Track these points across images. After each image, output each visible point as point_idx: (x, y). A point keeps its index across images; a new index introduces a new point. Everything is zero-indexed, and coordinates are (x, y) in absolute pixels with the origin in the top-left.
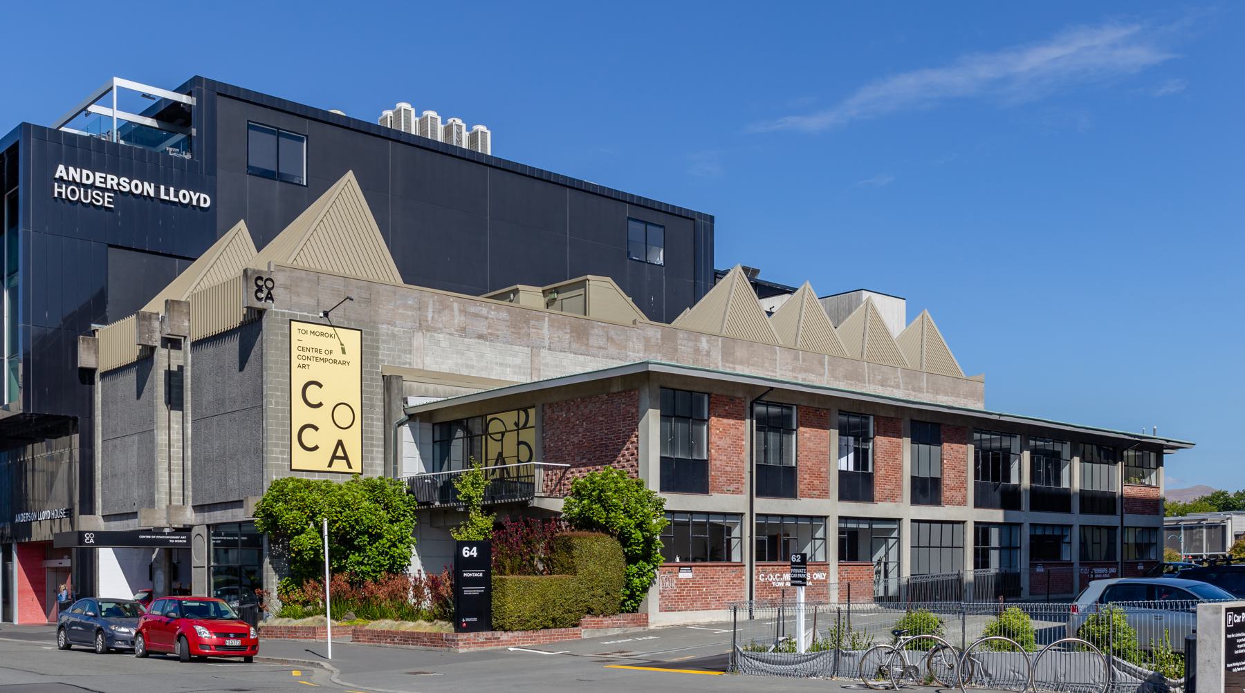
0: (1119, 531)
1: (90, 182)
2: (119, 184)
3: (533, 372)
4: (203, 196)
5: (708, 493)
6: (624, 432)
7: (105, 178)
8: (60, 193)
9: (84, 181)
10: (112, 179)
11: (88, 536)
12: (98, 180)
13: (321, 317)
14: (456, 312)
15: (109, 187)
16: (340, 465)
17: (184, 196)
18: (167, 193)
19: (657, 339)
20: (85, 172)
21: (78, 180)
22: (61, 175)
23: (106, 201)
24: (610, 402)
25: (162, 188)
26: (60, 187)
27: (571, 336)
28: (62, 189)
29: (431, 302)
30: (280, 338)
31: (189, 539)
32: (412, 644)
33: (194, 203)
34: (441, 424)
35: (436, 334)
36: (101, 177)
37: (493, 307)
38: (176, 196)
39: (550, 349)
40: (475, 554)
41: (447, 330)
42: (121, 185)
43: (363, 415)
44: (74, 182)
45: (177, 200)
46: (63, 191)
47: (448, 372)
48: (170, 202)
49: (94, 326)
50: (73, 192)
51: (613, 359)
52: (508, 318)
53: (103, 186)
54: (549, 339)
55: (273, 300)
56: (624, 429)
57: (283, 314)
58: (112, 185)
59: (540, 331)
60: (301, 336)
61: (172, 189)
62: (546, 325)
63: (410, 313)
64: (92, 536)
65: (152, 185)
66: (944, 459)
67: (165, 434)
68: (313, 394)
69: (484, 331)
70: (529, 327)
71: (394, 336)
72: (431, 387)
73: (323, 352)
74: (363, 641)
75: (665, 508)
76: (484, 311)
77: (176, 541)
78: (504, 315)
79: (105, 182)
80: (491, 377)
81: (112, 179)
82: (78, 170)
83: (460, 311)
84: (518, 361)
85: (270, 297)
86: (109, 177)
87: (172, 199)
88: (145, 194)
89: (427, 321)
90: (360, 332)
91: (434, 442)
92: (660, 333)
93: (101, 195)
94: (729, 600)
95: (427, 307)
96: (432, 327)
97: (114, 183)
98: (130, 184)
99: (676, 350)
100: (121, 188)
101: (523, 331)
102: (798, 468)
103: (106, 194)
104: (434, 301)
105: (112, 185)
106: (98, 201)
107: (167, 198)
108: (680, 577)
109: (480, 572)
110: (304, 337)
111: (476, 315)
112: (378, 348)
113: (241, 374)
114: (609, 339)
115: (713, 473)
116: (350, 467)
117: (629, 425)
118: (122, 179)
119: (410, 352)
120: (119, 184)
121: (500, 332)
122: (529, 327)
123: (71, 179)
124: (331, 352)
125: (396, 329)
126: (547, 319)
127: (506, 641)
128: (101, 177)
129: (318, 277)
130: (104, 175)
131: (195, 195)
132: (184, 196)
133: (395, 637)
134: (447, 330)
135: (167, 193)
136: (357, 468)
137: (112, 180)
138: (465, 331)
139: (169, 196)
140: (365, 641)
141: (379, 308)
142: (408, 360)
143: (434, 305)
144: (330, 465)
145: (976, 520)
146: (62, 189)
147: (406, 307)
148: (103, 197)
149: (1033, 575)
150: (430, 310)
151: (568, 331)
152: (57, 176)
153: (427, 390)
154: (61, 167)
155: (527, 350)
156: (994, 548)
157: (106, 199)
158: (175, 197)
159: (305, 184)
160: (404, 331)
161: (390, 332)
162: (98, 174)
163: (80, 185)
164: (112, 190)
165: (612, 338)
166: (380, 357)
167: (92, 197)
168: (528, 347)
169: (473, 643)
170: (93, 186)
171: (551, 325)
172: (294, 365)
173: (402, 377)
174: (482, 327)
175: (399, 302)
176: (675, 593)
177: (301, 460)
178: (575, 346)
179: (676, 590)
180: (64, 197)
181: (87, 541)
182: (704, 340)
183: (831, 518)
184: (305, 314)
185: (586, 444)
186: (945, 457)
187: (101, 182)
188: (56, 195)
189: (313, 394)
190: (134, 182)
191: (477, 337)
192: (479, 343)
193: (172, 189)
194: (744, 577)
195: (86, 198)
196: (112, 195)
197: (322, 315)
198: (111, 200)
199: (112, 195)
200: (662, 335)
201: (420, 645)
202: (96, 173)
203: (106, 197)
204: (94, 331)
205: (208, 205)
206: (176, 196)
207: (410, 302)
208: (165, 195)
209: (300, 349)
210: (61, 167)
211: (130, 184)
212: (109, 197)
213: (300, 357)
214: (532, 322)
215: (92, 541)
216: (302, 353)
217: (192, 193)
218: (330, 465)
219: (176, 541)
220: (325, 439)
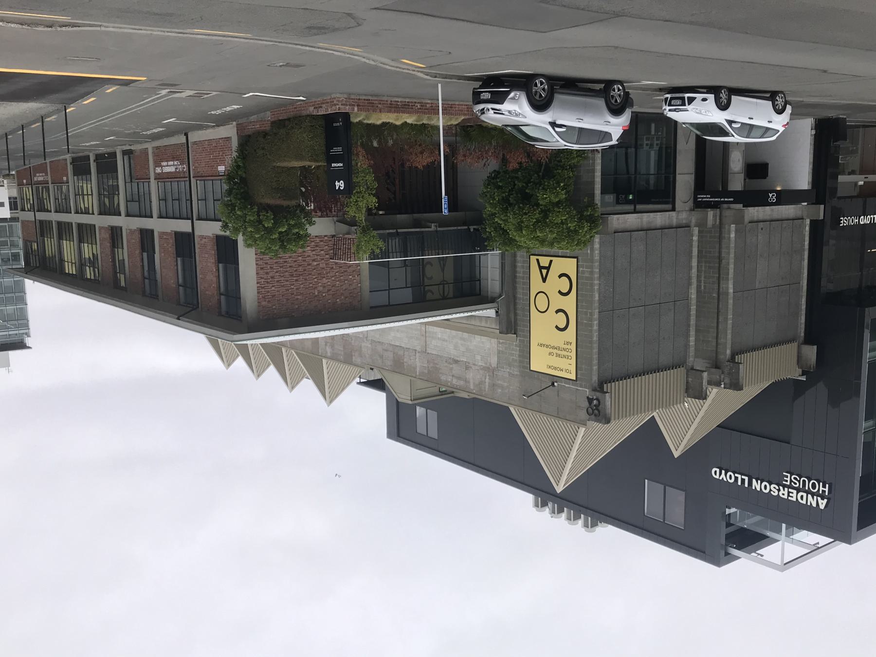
0: (36, 208)
1: (800, 494)
2: (779, 490)
3: (425, 334)
4: (717, 477)
5: (216, 236)
6: (273, 286)
7: (789, 496)
8: (824, 486)
9: (805, 495)
10: (783, 494)
11: (774, 200)
12: (794, 495)
13: (556, 382)
14: (471, 381)
15: (786, 489)
16: (545, 261)
17: (731, 478)
18: (743, 481)
19: (354, 356)
20: (804, 502)
21: (810, 496)
22: (822, 501)
23: (788, 479)
24: (289, 310)
25: (746, 485)
26: (824, 491)
27: (403, 360)
28: (822, 490)
29: (487, 390)
30: (583, 366)
31: (695, 198)
32: (398, 102)
33: (723, 472)
34: (476, 295)
35: (484, 365)
36: (792, 497)
37: (449, 384)
38: (736, 478)
39: (416, 350)
40: (337, 183)
41: (477, 367)
42: (777, 490)
43: (528, 303)
44: (813, 495)
45: (736, 475)
46: (821, 488)
47: (476, 336)
48: (742, 474)
49: (804, 378)
50: (814, 486)
51: (379, 342)
52: (440, 375)
53: (790, 490)
54: (416, 359)
55: (588, 397)
56: (273, 288)
57: (581, 387)
58: (784, 490)
59: (422, 365)
60: (569, 367)
61: (739, 483)
62: (418, 370)
63: (499, 382)
64: (770, 200)
65: (754, 488)
66: (112, 262)
67: (723, 288)
68: (561, 321)
69: (454, 366)
70: (428, 367)
71: (510, 365)
72: (483, 324)
73: (555, 354)
74: (462, 105)
75: (220, 223)
76: (455, 381)
77: (705, 196)
78: (443, 378)
79: (789, 492)
80: (450, 330)
81: (783, 494)
82: (809, 504)
83: (469, 382)
84: (434, 342)
85: (590, 400)
86: (785, 497)
87: (739, 476)
88: (759, 481)
89: (489, 375)
90: (531, 369)
91: (480, 280)
92: (353, 360)
93: (792, 483)
94: (199, 148)
95: (489, 386)
96: (485, 370)
97: (782, 492)
98: (771, 490)
99: (344, 347)
100: (777, 488)
101: (432, 365)
102: (175, 256)
103: (788, 483)
104: (485, 391)
105: (784, 490)
106: (795, 478)
107: (743, 477)
108: (224, 167)
109: (333, 167)
110: (567, 368)
111: (459, 378)
112: (520, 356)
113: (33, 348)
114: (381, 357)
115: (213, 252)
116: (538, 260)
117: (268, 292)
118: (776, 494)
119: (499, 352)
120: (779, 490)
121: (445, 365)
122: (428, 367)
123: (815, 497)
124: (550, 354)
125: (508, 370)
126: (418, 374)
127: (310, 106)
128: (792, 497)
129: (558, 414)
130: (790, 498)
131: (723, 478)
132: (731, 478)
133: (420, 109)
134: (477, 367)
135: (743, 481)
136: (533, 259)
137: (784, 493)
138: (466, 367)
139: (742, 479)
140: (458, 105)
141: (519, 387)
142: (500, 345)
143: (485, 388)
144: (551, 261)
145: (70, 214)
146: (822, 490)
147: (502, 387)
148: (791, 481)
149: (67, 176)
150: (487, 384)
151: (405, 364)
152: (826, 500)
153: (486, 322)
154: (822, 507)
155: (429, 351)
156: (635, 207)
157: (789, 479)
158: (738, 477)
159: (646, 481)
160: (503, 368)
161: (512, 368)
162: (794, 499)
163: (808, 492)
164: (784, 486)
165: (380, 357)
166: (518, 349)
167: (799, 481)
168: (428, 353)
169: (328, 103)
170: (798, 490)
171: (415, 368)
172: (574, 346)
173: (500, 333)
174: (457, 370)
175: (506, 391)
176: (226, 153)
177: (569, 266)
178: (401, 353)
179: (226, 155)
180: (821, 484)
181: (774, 195)
182: (329, 354)
183: (156, 217)
184: (567, 385)
185: (314, 277)
186: (111, 264)
187: (792, 493)
188: (827, 485)
189: (561, 321)
190: (767, 491)
191: (459, 361)
192: (457, 357)
193: (739, 483)
194: (193, 167)
195: (804, 481)
196: (784, 482)
197: (556, 384)
198: (785, 478)
199: (784, 482)
200: (352, 359)
201: (387, 101)
202: (795, 500)
203: (789, 481)
204: (803, 375)
205: (714, 470)
206: (736, 478)
207: (500, 390)
208: (744, 479)
209: (570, 358)
210: (822, 507)
211: (771, 490)
212: (787, 481)
213: (570, 351)
214: (426, 371)
215: (770, 195)
216: (569, 354)
217: (725, 480)
218: (551, 261)
219: (705, 196)
220: (556, 284)
